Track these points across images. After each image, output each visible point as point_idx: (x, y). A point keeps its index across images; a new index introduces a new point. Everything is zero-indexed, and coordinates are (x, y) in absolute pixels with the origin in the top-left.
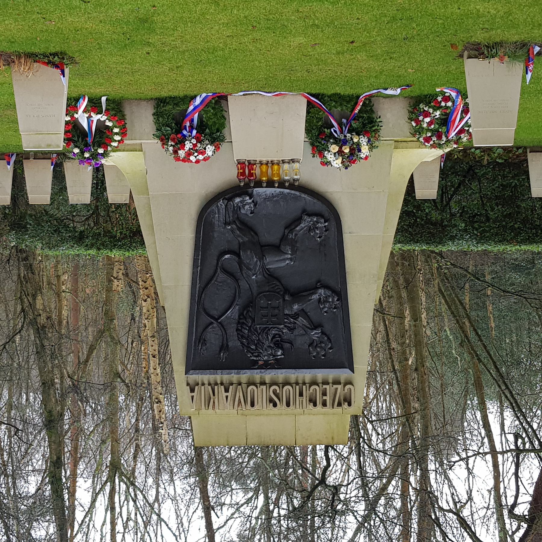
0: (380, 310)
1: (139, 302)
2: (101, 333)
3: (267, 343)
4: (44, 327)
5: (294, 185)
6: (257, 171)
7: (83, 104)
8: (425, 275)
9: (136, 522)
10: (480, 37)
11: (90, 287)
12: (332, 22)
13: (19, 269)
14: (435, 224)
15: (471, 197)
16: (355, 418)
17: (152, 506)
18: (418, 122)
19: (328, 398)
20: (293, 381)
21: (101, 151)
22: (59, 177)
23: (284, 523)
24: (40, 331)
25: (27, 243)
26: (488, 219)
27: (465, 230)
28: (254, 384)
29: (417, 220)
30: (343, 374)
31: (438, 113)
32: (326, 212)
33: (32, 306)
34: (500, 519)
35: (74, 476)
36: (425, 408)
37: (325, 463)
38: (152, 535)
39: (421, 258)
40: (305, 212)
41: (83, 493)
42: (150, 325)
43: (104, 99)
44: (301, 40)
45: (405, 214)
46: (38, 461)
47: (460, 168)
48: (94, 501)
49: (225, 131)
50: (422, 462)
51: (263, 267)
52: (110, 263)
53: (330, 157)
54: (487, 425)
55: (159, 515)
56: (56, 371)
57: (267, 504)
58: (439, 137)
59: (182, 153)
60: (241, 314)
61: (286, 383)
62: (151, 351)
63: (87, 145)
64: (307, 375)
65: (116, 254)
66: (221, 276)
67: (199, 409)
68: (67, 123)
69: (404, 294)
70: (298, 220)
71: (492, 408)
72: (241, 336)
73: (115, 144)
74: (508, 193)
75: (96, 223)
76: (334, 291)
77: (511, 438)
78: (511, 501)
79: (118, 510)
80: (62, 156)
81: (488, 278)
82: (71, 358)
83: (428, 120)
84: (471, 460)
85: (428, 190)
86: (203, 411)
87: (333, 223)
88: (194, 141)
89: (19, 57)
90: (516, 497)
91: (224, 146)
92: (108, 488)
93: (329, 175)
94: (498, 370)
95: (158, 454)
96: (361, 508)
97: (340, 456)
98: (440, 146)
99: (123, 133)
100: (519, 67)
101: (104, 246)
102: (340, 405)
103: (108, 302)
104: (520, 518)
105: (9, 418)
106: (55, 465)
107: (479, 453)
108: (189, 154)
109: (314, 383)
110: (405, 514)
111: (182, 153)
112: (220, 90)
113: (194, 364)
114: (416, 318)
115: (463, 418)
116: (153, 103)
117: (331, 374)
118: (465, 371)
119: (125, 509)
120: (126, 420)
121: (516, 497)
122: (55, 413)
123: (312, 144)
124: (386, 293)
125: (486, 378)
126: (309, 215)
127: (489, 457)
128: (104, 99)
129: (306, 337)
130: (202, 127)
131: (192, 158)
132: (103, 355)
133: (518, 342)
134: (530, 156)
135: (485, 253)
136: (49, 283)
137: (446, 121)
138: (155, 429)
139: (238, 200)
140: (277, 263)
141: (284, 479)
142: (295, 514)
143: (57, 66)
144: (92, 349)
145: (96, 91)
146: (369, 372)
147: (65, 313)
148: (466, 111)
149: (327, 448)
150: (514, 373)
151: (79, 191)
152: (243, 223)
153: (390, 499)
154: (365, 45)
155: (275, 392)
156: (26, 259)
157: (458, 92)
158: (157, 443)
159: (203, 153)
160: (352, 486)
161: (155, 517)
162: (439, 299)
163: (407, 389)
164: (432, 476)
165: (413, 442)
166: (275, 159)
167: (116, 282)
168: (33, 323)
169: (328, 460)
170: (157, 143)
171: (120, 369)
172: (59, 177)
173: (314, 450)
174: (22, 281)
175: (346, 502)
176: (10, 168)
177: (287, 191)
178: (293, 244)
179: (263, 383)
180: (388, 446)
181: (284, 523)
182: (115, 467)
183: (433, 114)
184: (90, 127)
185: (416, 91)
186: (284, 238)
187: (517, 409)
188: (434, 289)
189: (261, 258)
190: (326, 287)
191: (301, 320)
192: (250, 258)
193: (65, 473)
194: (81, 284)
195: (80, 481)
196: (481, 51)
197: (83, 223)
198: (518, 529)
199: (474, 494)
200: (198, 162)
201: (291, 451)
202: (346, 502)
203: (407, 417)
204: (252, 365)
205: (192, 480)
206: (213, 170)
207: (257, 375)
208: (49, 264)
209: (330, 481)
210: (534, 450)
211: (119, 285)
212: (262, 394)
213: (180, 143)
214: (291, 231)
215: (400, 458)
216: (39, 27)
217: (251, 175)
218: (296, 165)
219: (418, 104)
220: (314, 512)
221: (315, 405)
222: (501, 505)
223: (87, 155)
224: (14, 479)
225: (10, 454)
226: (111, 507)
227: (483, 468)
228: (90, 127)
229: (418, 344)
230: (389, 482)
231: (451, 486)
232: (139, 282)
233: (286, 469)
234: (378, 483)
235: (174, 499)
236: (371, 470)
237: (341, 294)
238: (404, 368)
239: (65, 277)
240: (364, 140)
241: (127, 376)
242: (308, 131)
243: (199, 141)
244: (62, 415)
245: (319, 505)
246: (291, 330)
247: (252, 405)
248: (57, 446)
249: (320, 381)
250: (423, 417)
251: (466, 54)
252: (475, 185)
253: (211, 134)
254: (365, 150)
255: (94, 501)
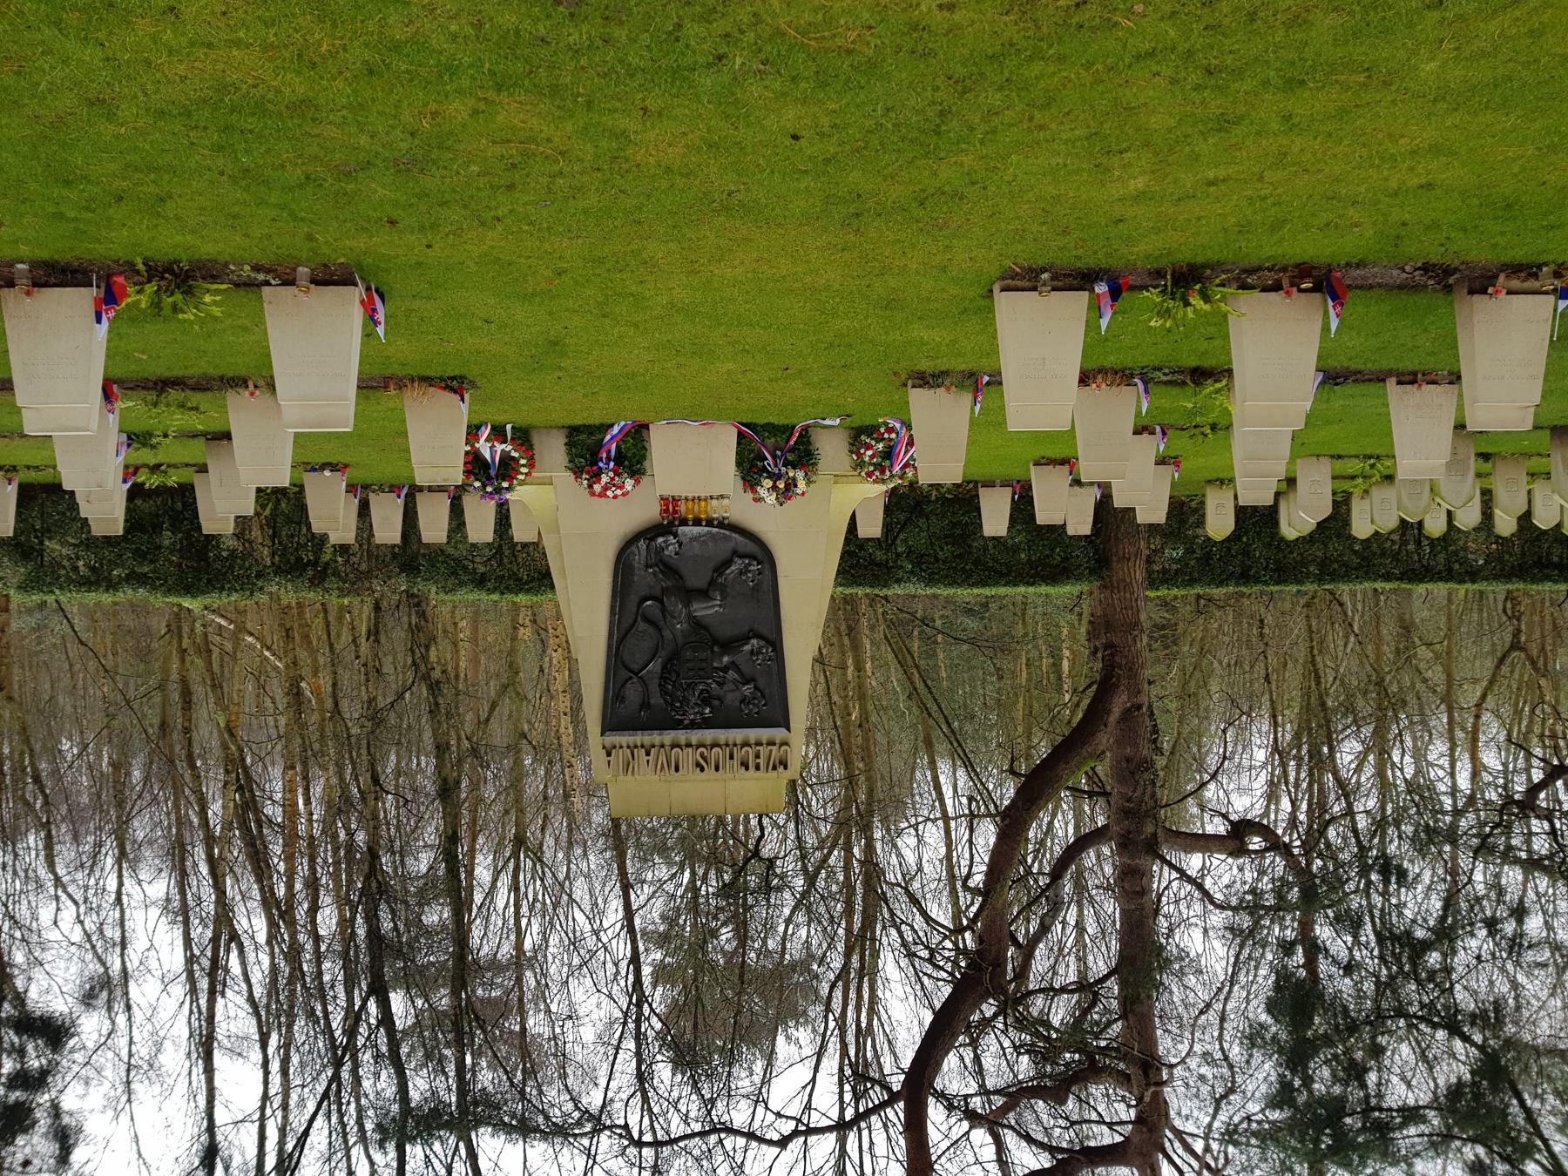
0: (820, 660)
1: (549, 651)
2: (505, 687)
3: (694, 700)
4: (438, 682)
5: (722, 524)
6: (682, 508)
7: (486, 432)
8: (869, 620)
9: (544, 904)
10: (925, 365)
11: (492, 634)
12: (764, 348)
13: (410, 616)
14: (879, 565)
15: (916, 537)
16: (793, 783)
17: (562, 885)
18: (859, 455)
19: (761, 761)
20: (722, 742)
21: (505, 484)
22: (457, 511)
23: (713, 902)
24: (434, 687)
25: (420, 586)
26: (937, 560)
27: (912, 572)
28: (679, 746)
29: (860, 563)
30: (778, 733)
31: (881, 446)
32: (760, 554)
33: (425, 658)
34: (953, 893)
35: (472, 853)
36: (869, 770)
37: (758, 833)
38: (562, 918)
39: (865, 601)
40: (736, 553)
41: (483, 873)
42: (560, 680)
43: (509, 427)
44: (731, 366)
45: (846, 555)
46: (431, 834)
47: (907, 505)
48: (495, 881)
49: (646, 464)
50: (866, 829)
51: (689, 614)
52: (516, 608)
53: (763, 492)
54: (938, 787)
55: (570, 896)
56: (452, 733)
57: (693, 880)
58: (883, 472)
59: (597, 488)
60: (664, 667)
61: (715, 745)
62: (562, 708)
63: (489, 478)
64: (737, 735)
65: (522, 599)
66: (642, 626)
67: (616, 776)
68: (467, 453)
69: (846, 641)
70: (728, 563)
71: (944, 767)
72: (664, 692)
73: (521, 477)
74: (958, 532)
75: (501, 564)
76: (768, 642)
77: (964, 801)
78: (965, 871)
79: (523, 889)
80: (462, 488)
81: (938, 623)
82: (469, 717)
83: (870, 453)
84: (921, 827)
85: (871, 528)
86: (621, 777)
87: (767, 566)
88: (611, 474)
89: (412, 380)
90: (971, 867)
91: (645, 480)
92: (511, 865)
93: (761, 512)
94: (949, 725)
95: (569, 825)
96: (799, 883)
97: (775, 824)
98: (884, 481)
99: (531, 465)
100: (967, 398)
101: (509, 590)
102: (774, 768)
103: (512, 652)
104: (975, 891)
105: (397, 786)
106: (450, 840)
107: (928, 819)
108: (606, 488)
109: (746, 744)
110: (848, 886)
111: (597, 488)
112: (641, 418)
113: (611, 724)
114: (859, 668)
115: (912, 779)
116: (565, 431)
117: (764, 734)
118: (914, 726)
119: (533, 889)
120: (533, 787)
121: (971, 867)
122: (451, 781)
123: (743, 478)
124: (827, 640)
125: (936, 734)
126: (741, 556)
127: (940, 823)
128: (509, 427)
129: (737, 693)
130: (620, 459)
131: (609, 493)
132: (507, 712)
133: (972, 694)
134: (982, 491)
135: (935, 596)
136: (445, 631)
137: (889, 454)
138: (566, 796)
139: (660, 540)
140: (705, 610)
141: (713, 851)
142: (725, 891)
143: (455, 392)
144: (493, 706)
145: (499, 418)
146: (809, 729)
147: (462, 664)
148: (911, 444)
149: (761, 817)
150: (968, 728)
151: (480, 528)
152: (665, 565)
153: (831, 874)
154: (800, 372)
155: (702, 755)
156: (418, 605)
157: (903, 423)
158: (568, 813)
159: (621, 488)
160: (790, 858)
161: (565, 897)
162: (884, 647)
163: (850, 748)
164: (878, 845)
165: (857, 808)
166: (703, 495)
167: (522, 630)
168: (426, 677)
169: (762, 829)
170: (570, 476)
171: (526, 727)
172: (457, 511)
173: (747, 820)
174: (414, 630)
175: (782, 877)
176: (401, 502)
177: (715, 530)
178: (723, 590)
179: (689, 745)
180: (830, 811)
181: (713, 902)
182: (520, 841)
183: (874, 443)
184: (493, 459)
185: (857, 422)
186: (712, 583)
187: (969, 765)
188: (879, 635)
189: (687, 605)
190: (759, 636)
191: (732, 674)
192: (675, 605)
193: (462, 850)
194: (481, 630)
195: (479, 858)
196: (925, 380)
197: (484, 564)
198: (972, 903)
199: (925, 865)
200: (615, 497)
201: (721, 821)
202: (782, 877)
203: (851, 780)
204: (677, 725)
205: (608, 854)
206: (632, 507)
207: (681, 736)
208: (445, 610)
209: (766, 852)
210: (989, 815)
211: (525, 633)
212: (688, 757)
213: (596, 476)
214: (721, 575)
215: (842, 824)
216: (435, 349)
217: (675, 512)
218: (726, 502)
219: (859, 435)
220: (746, 889)
221: (747, 769)
222: (954, 876)
223: (489, 489)
224: (402, 857)
225: (398, 828)
226: (515, 887)
227: (933, 834)
228: (493, 459)
229: (862, 697)
230: (830, 853)
231: (899, 855)
232: (548, 631)
233: (715, 841)
234: (818, 854)
235: (587, 876)
236: (810, 840)
237: (775, 643)
238: (847, 724)
239: (463, 624)
240: (800, 475)
241: (535, 737)
242: (739, 464)
243: (617, 474)
244: (458, 782)
245: (753, 881)
246: (720, 685)
247: (677, 770)
248: (452, 818)
249: (752, 741)
250: (868, 779)
251: (910, 383)
252: (922, 522)
253: (630, 467)
254: (801, 485)
255: (495, 881)
